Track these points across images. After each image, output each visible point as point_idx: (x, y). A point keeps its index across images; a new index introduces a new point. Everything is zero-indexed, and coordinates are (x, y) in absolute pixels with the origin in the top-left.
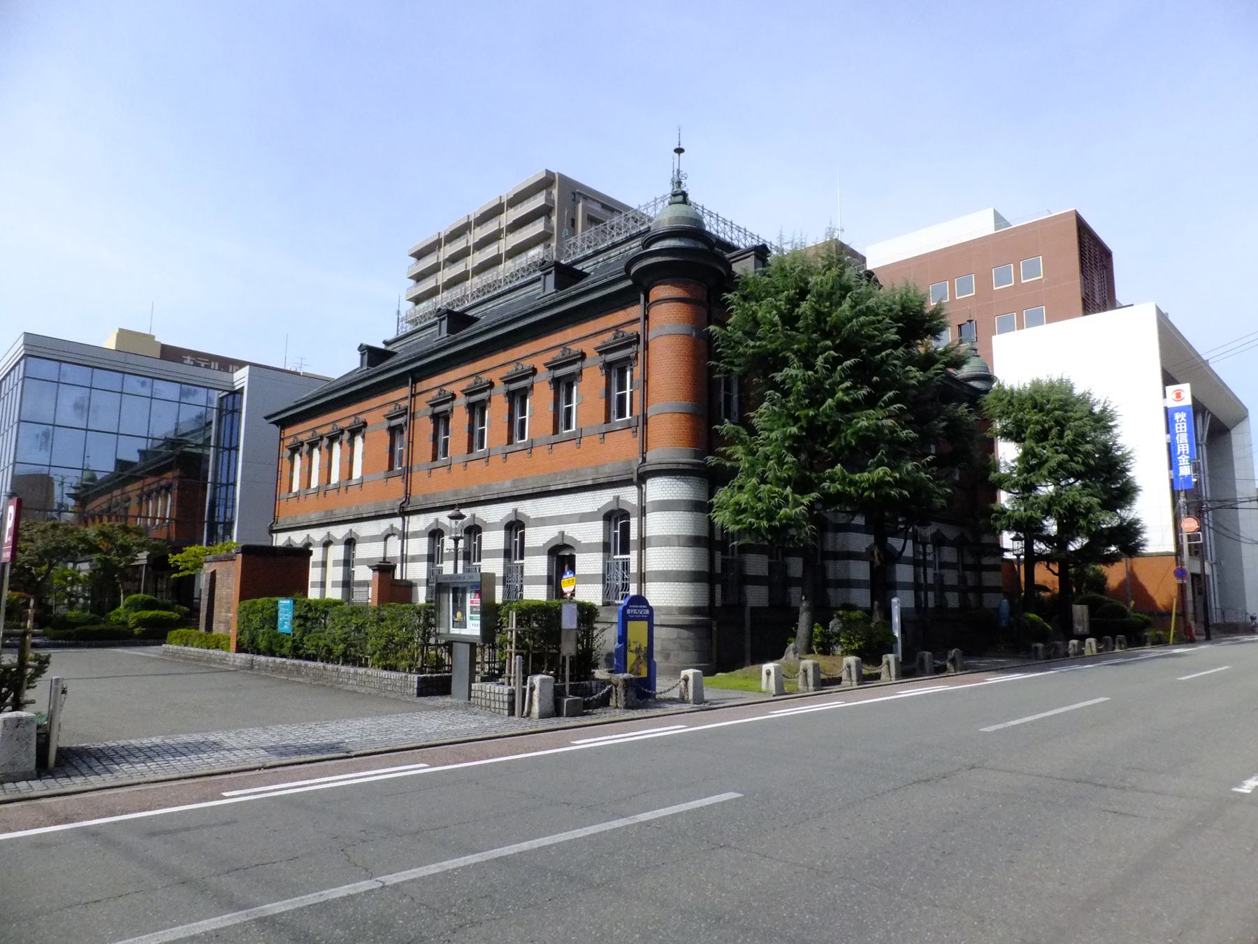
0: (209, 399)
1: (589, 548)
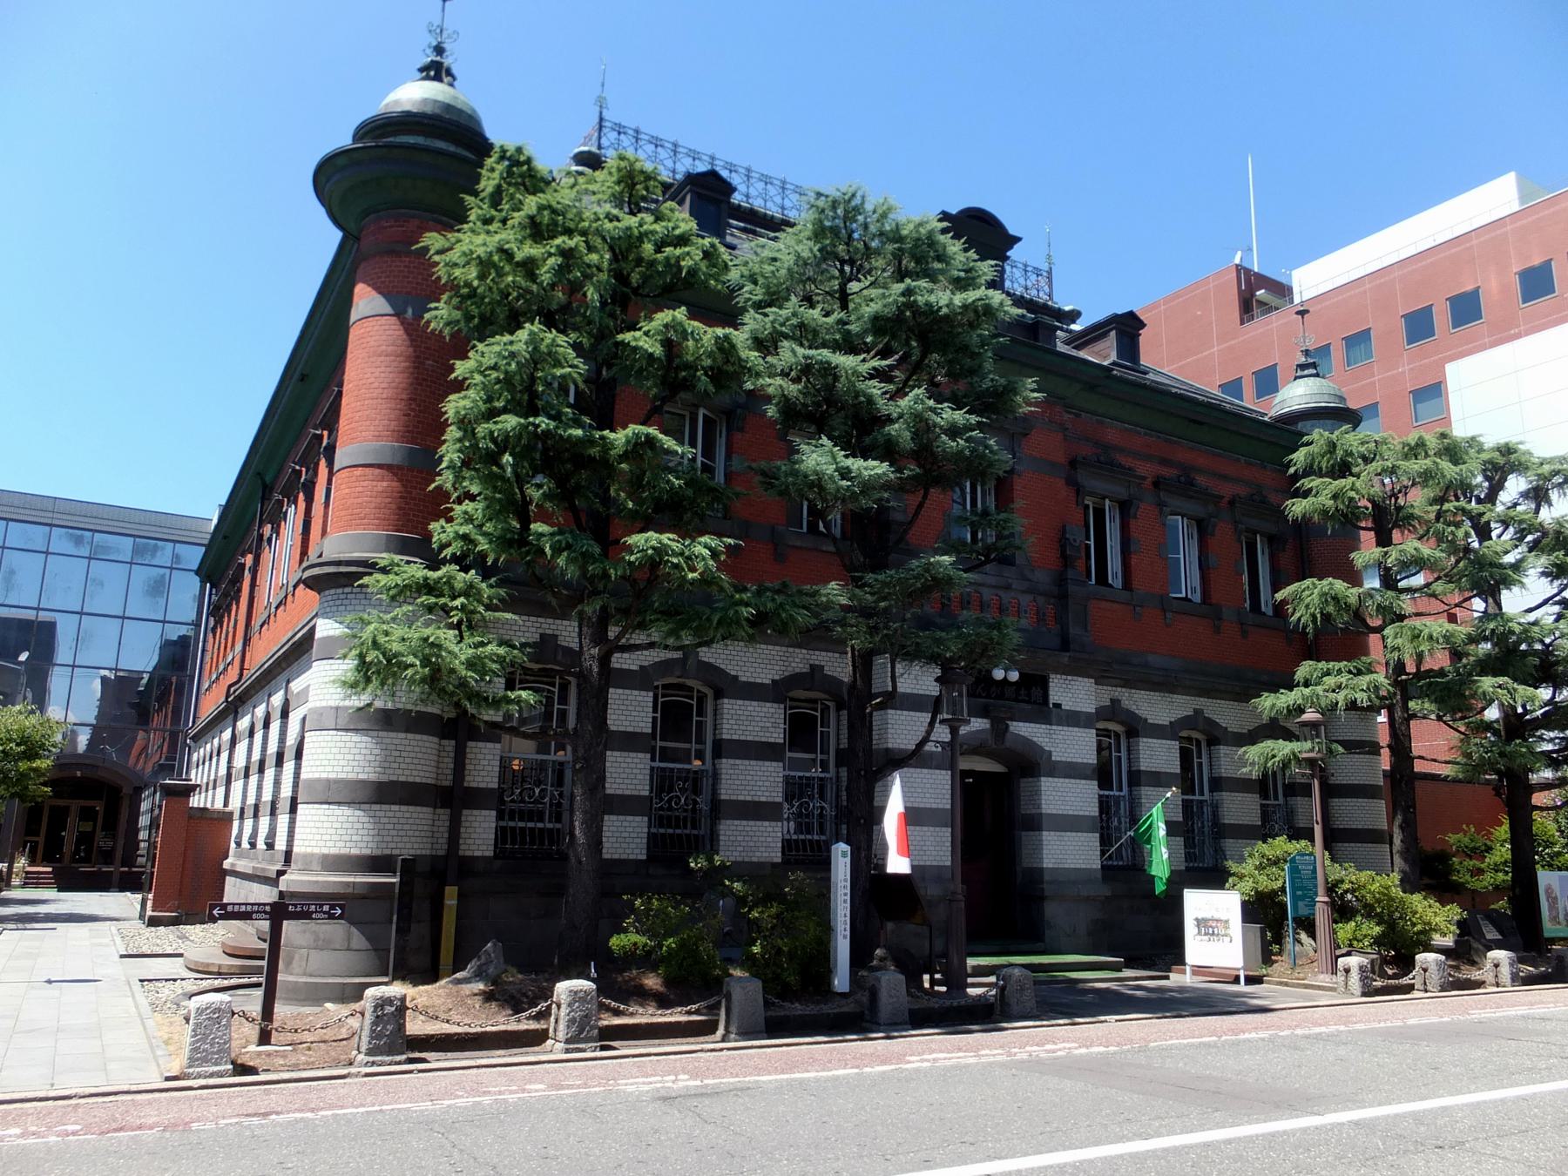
0: (176, 557)
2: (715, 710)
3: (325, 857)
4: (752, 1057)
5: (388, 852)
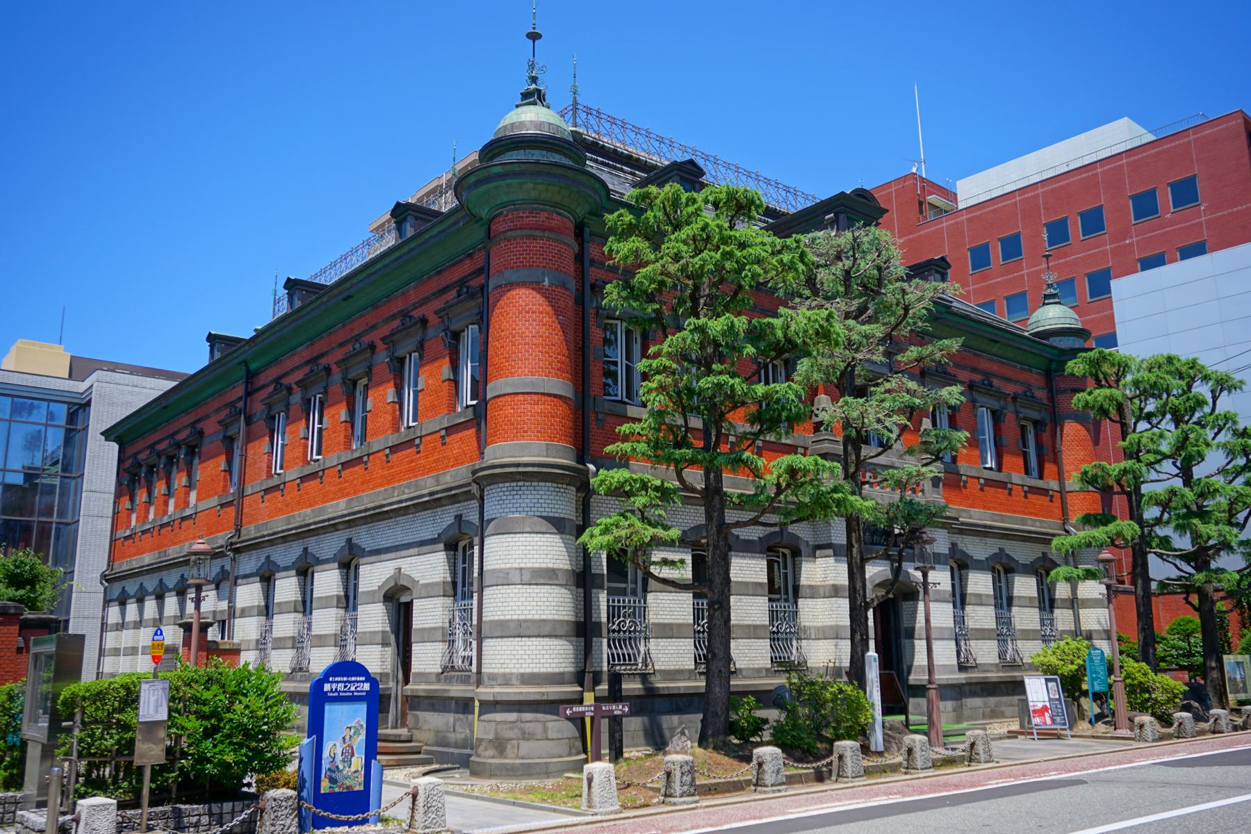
0: (51, 416)
1: (429, 591)
2: (794, 564)
3: (522, 675)
4: (713, 813)
5: (562, 670)
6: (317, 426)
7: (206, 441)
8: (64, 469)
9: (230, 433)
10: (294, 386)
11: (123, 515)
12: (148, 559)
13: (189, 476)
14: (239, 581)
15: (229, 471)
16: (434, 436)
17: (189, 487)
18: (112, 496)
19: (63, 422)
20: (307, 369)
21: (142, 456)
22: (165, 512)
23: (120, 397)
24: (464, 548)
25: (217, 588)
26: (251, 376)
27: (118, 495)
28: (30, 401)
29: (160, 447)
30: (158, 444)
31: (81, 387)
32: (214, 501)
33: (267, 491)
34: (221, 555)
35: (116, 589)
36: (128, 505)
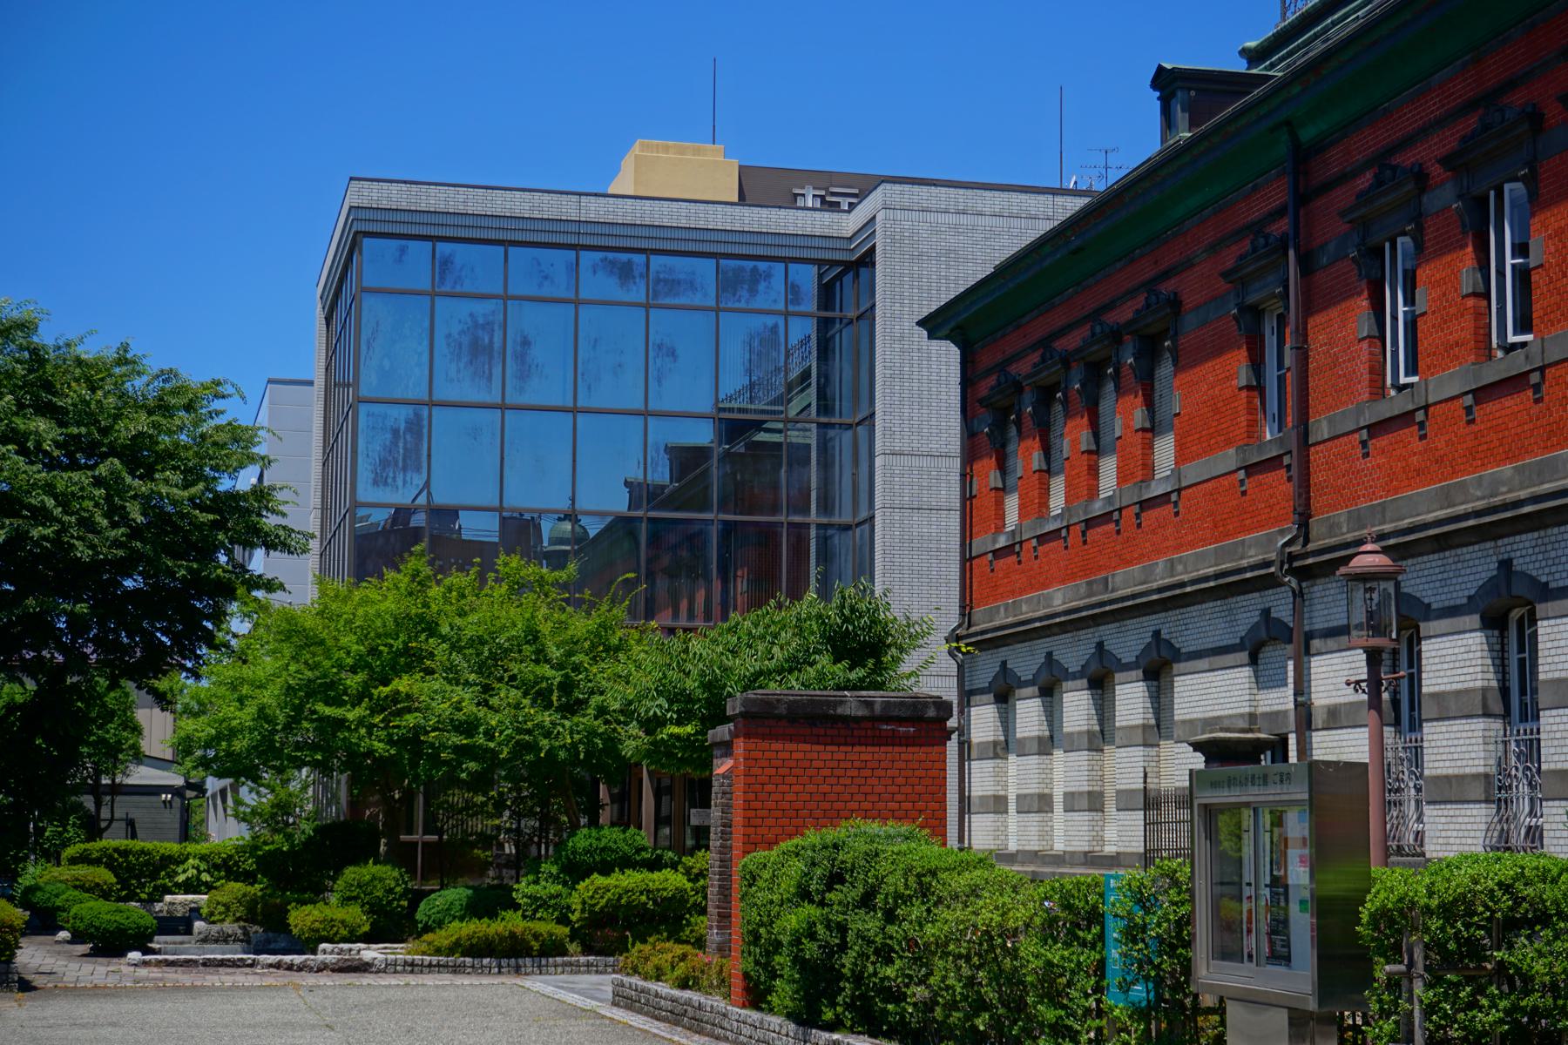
0: (793, 291)
6: (1401, 309)
7: (1190, 321)
8: (825, 406)
9: (1252, 299)
10: (1436, 170)
11: (985, 503)
12: (1059, 599)
13: (1149, 404)
14: (1316, 644)
15: (1257, 388)
16: (1225, 482)
17: (1152, 430)
18: (957, 464)
19: (810, 305)
20: (1473, 121)
21: (1022, 368)
22: (1093, 492)
23: (943, 242)
24: (1520, 622)
25: (1254, 661)
26: (1302, 157)
27: (970, 455)
28: (750, 264)
29: (1061, 345)
30: (1042, 343)
31: (849, 224)
32: (1228, 459)
33: (1376, 429)
34: (1267, 583)
35: (986, 669)
36: (994, 479)
